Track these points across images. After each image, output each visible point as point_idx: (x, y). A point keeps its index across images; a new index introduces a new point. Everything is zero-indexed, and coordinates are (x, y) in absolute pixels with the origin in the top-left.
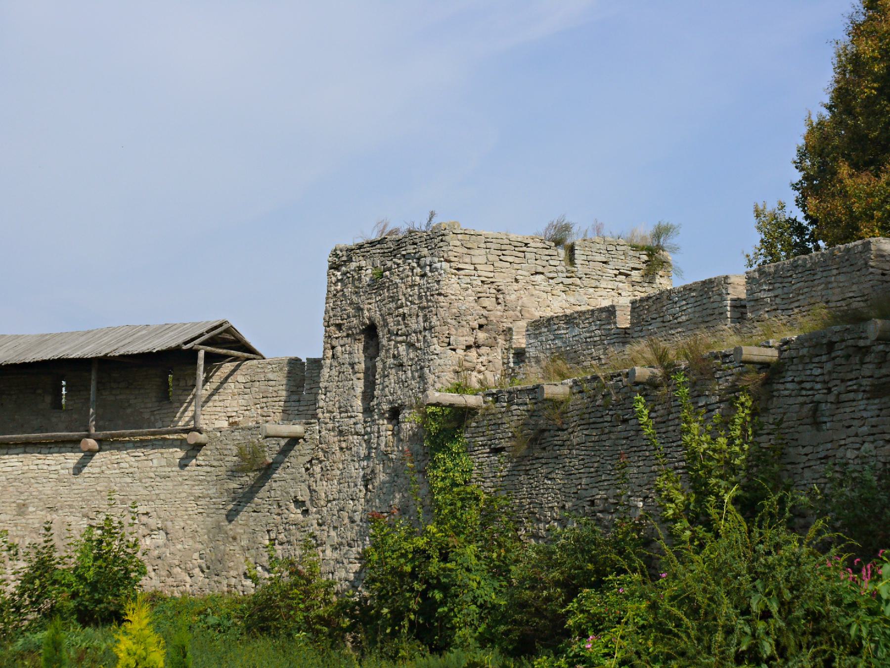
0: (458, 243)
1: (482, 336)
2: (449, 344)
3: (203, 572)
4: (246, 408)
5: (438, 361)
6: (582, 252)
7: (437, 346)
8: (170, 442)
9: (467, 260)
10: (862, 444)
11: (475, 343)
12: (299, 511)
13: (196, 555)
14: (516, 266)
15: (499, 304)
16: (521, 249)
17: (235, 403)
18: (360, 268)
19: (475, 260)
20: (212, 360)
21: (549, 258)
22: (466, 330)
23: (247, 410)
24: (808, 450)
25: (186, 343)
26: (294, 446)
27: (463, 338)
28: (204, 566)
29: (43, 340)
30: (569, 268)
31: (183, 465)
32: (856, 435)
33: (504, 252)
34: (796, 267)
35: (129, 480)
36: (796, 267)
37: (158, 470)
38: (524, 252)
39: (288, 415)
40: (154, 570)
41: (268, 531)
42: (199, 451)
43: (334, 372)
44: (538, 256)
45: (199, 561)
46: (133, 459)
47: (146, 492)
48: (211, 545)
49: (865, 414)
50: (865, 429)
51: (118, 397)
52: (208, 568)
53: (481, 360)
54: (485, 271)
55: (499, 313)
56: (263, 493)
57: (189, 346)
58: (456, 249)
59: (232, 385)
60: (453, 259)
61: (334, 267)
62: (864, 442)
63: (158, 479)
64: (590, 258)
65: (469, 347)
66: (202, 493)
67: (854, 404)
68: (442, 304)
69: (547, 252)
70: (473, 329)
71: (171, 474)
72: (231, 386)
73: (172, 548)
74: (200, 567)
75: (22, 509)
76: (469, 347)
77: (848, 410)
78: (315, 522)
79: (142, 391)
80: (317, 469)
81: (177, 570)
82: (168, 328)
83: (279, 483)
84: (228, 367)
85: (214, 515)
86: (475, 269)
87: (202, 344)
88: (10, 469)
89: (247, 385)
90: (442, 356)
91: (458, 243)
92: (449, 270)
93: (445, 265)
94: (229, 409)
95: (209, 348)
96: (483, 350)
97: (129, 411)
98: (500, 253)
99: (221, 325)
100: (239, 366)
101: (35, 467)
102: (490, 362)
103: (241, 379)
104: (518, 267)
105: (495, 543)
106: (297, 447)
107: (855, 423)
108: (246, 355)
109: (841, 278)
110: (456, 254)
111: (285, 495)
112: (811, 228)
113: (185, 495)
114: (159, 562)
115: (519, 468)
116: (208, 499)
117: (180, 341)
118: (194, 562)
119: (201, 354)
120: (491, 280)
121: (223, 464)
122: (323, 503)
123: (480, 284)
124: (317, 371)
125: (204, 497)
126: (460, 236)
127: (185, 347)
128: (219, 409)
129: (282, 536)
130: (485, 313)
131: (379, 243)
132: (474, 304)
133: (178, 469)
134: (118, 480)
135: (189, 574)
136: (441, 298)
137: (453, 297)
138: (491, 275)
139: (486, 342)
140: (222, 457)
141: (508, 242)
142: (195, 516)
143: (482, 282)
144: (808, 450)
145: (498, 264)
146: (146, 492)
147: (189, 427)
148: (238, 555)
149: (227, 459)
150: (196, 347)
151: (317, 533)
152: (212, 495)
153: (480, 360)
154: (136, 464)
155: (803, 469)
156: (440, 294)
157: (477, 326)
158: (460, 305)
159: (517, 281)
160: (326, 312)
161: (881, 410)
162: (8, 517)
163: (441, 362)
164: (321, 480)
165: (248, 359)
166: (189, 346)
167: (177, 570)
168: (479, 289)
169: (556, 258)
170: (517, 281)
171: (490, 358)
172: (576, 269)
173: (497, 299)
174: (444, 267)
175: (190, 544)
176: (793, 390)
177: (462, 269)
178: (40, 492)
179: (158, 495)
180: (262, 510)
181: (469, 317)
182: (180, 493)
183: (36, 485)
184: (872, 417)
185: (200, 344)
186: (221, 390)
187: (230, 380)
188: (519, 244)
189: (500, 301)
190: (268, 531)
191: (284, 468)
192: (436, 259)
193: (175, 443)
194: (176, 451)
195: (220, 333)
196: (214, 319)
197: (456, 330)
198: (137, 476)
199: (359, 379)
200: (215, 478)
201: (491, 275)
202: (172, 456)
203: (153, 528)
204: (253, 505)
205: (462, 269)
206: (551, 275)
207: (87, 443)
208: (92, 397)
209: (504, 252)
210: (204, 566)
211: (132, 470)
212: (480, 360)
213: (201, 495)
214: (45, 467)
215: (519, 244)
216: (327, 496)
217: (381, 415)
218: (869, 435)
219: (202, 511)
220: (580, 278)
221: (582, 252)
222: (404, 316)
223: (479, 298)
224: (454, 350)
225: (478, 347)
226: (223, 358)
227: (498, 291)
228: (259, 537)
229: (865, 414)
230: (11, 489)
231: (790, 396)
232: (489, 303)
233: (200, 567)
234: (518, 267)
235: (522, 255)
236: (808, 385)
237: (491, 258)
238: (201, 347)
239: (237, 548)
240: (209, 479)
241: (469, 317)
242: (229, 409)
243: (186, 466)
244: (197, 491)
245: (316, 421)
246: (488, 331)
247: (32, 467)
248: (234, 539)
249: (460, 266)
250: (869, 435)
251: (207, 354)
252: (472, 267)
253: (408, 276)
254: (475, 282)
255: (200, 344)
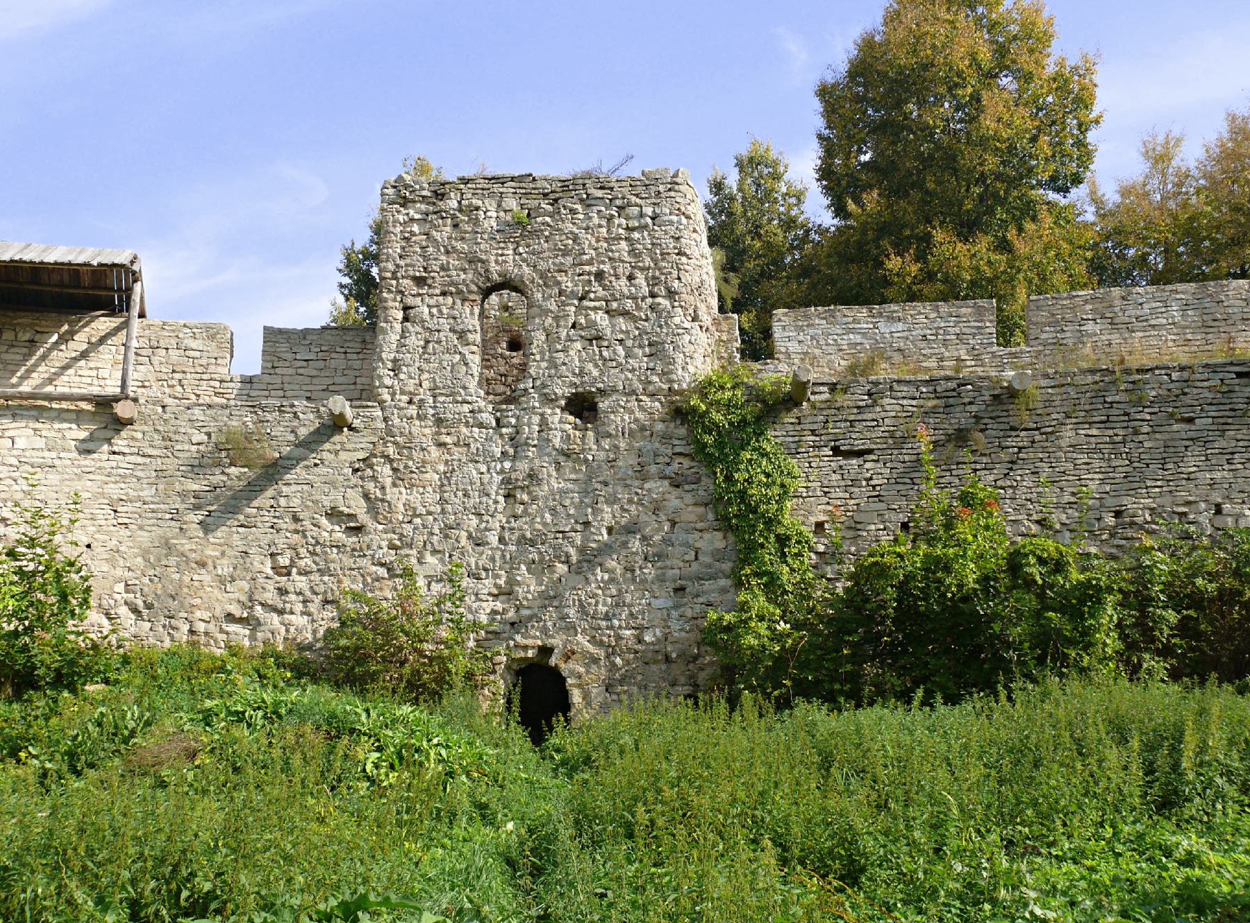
4: (140, 384)
8: (54, 414)
13: (120, 587)
23: (144, 387)
26: (332, 436)
31: (85, 449)
37: (27, 454)
42: (118, 431)
45: (125, 595)
48: (152, 572)
52: (149, 606)
56: (264, 500)
66: (127, 494)
71: (57, 462)
83: (294, 488)
85: (154, 528)
106: (337, 438)
111: (310, 504)
116: (138, 504)
118: (117, 597)
121: (170, 455)
124: (25, 350)
131: (512, 181)
133: (75, 455)
135: (107, 614)
140: (169, 443)
142: (112, 528)
148: (209, 589)
149: (179, 447)
152: (147, 499)
164: (394, 485)
175: (105, 569)
180: (259, 524)
191: (307, 467)
193: (64, 415)
194: (70, 428)
199: (473, 353)
200: (154, 474)
202: (60, 435)
204: (241, 517)
210: (140, 603)
213: (124, 497)
217: (548, 400)
228: (255, 563)
243: (89, 452)
244: (114, 490)
245: (376, 404)
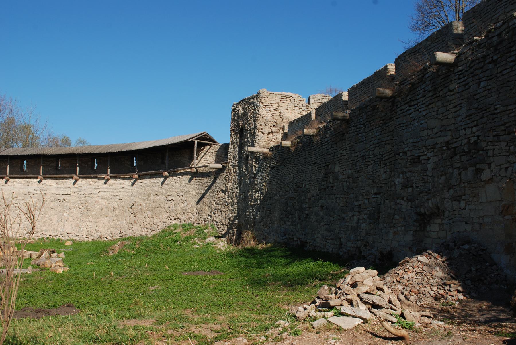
0: (265, 96)
1: (274, 129)
2: (262, 132)
3: (197, 214)
5: (258, 138)
6: (312, 99)
7: (258, 133)
9: (269, 102)
10: (375, 148)
11: (271, 131)
12: (223, 193)
14: (287, 104)
15: (281, 118)
16: (289, 98)
17: (210, 159)
18: (239, 109)
19: (271, 102)
20: (201, 146)
21: (300, 101)
25: (190, 139)
27: (267, 130)
28: (197, 212)
30: (308, 105)
33: (283, 99)
34: (363, 83)
35: (177, 185)
36: (363, 83)
38: (290, 99)
39: (217, 162)
40: (184, 214)
41: (215, 200)
43: (232, 146)
44: (295, 101)
46: (178, 178)
47: (181, 189)
49: (376, 135)
51: (178, 159)
53: (274, 137)
54: (275, 106)
55: (280, 121)
57: (191, 140)
58: (264, 98)
59: (209, 153)
60: (263, 102)
61: (233, 110)
62: (376, 147)
63: (185, 184)
64: (315, 101)
65: (269, 133)
67: (373, 131)
68: (260, 118)
69: (299, 99)
70: (271, 127)
72: (209, 154)
73: (189, 207)
74: (196, 213)
76: (269, 133)
77: (371, 134)
78: (227, 197)
79: (185, 157)
80: (228, 179)
81: (190, 214)
84: (207, 147)
86: (272, 105)
87: (196, 139)
88: (146, 183)
89: (213, 153)
90: (259, 136)
91: (265, 96)
92: (262, 106)
93: (261, 104)
94: (208, 161)
95: (198, 141)
96: (275, 134)
97: (181, 163)
98: (281, 100)
99: (204, 133)
100: (211, 147)
101: (153, 182)
102: (277, 138)
103: (212, 151)
104: (288, 104)
107: (373, 139)
108: (212, 143)
110: (265, 100)
113: (192, 189)
114: (185, 211)
115: (278, 174)
119: (196, 143)
120: (277, 109)
122: (229, 190)
123: (273, 110)
125: (197, 190)
126: (266, 94)
127: (189, 140)
128: (205, 161)
129: (218, 202)
130: (275, 121)
132: (271, 118)
134: (174, 185)
136: (259, 116)
137: (263, 115)
138: (278, 107)
139: (276, 131)
141: (284, 96)
143: (274, 110)
145: (280, 103)
146: (181, 189)
147: (85, 147)
150: (193, 140)
151: (227, 201)
153: (273, 138)
154: (179, 180)
155: (356, 162)
156: (259, 115)
157: (272, 126)
158: (266, 118)
159: (287, 109)
160: (231, 125)
161: (381, 131)
162: (146, 198)
163: (259, 138)
165: (214, 145)
166: (191, 140)
167: (190, 214)
168: (273, 112)
169: (303, 101)
170: (287, 109)
171: (277, 137)
172: (310, 105)
173: (280, 116)
174: (260, 105)
176: (354, 130)
177: (267, 106)
178: (154, 189)
179: (185, 189)
181: (269, 122)
182: (191, 188)
183: (153, 188)
184: (378, 135)
185: (195, 139)
186: (206, 155)
187: (208, 152)
188: (288, 96)
189: (281, 117)
190: (215, 200)
192: (258, 103)
195: (203, 136)
197: (265, 127)
198: (179, 183)
201: (278, 107)
203: (184, 200)
205: (267, 106)
206: (300, 107)
207: (165, 173)
209: (283, 99)
210: (197, 212)
211: (178, 182)
212: (273, 138)
214: (155, 182)
215: (288, 96)
216: (230, 188)
218: (377, 143)
219: (197, 194)
220: (312, 108)
221: (312, 99)
222: (249, 124)
223: (273, 115)
224: (264, 134)
225: (273, 133)
226: (206, 145)
227: (281, 113)
229: (376, 135)
230: (146, 189)
231: (353, 132)
232: (277, 117)
233: (196, 213)
234: (288, 104)
235: (289, 100)
236: (358, 127)
237: (277, 101)
238: (195, 140)
239: (206, 206)
240: (199, 184)
241: (269, 122)
242: (208, 161)
246: (276, 127)
247: (152, 182)
248: (206, 203)
249: (266, 104)
250: (377, 143)
251: (198, 143)
252: (271, 105)
253: (251, 110)
254: (271, 110)
255: (195, 139)
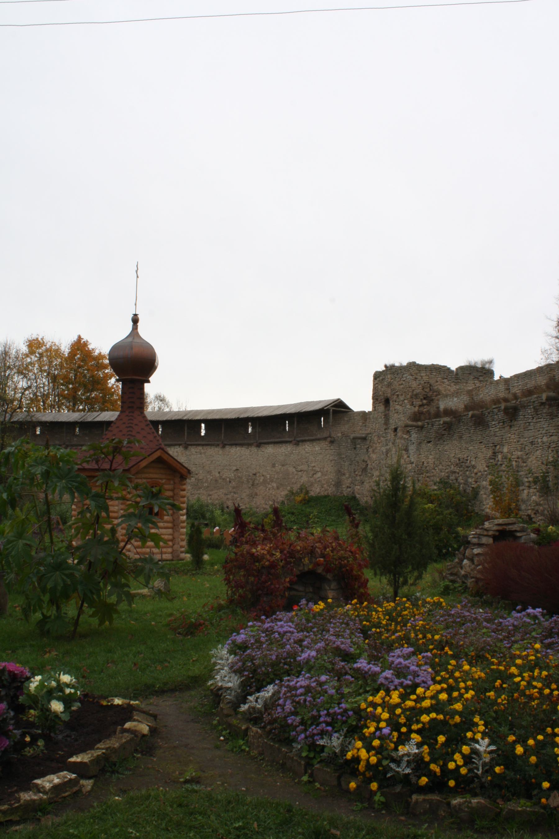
22: (419, 400)
24: (526, 439)
29: (296, 405)
32: (541, 434)
50: (544, 432)
75: (274, 466)
82: (320, 402)
105: (410, 826)
107: (541, 429)
109: (540, 378)
112: (47, 544)
117: (102, 414)
144: (526, 439)
196: (335, 397)
208: (295, 426)
229: (544, 426)
244: (331, 458)
251: (333, 410)
